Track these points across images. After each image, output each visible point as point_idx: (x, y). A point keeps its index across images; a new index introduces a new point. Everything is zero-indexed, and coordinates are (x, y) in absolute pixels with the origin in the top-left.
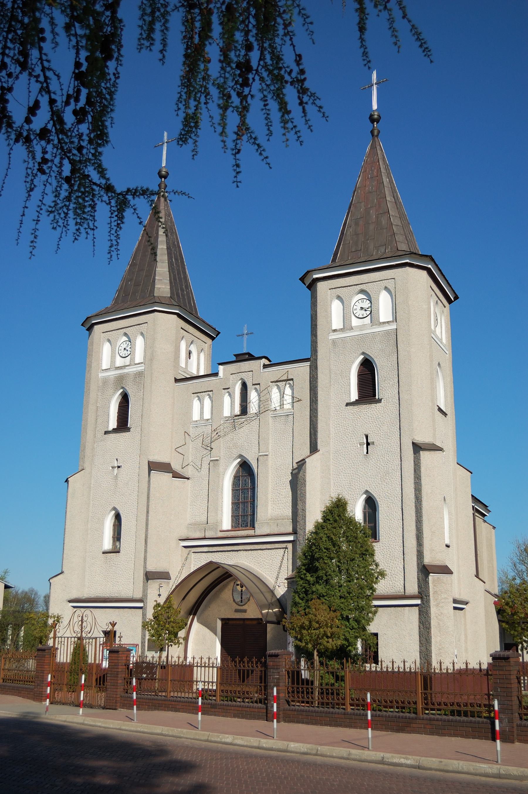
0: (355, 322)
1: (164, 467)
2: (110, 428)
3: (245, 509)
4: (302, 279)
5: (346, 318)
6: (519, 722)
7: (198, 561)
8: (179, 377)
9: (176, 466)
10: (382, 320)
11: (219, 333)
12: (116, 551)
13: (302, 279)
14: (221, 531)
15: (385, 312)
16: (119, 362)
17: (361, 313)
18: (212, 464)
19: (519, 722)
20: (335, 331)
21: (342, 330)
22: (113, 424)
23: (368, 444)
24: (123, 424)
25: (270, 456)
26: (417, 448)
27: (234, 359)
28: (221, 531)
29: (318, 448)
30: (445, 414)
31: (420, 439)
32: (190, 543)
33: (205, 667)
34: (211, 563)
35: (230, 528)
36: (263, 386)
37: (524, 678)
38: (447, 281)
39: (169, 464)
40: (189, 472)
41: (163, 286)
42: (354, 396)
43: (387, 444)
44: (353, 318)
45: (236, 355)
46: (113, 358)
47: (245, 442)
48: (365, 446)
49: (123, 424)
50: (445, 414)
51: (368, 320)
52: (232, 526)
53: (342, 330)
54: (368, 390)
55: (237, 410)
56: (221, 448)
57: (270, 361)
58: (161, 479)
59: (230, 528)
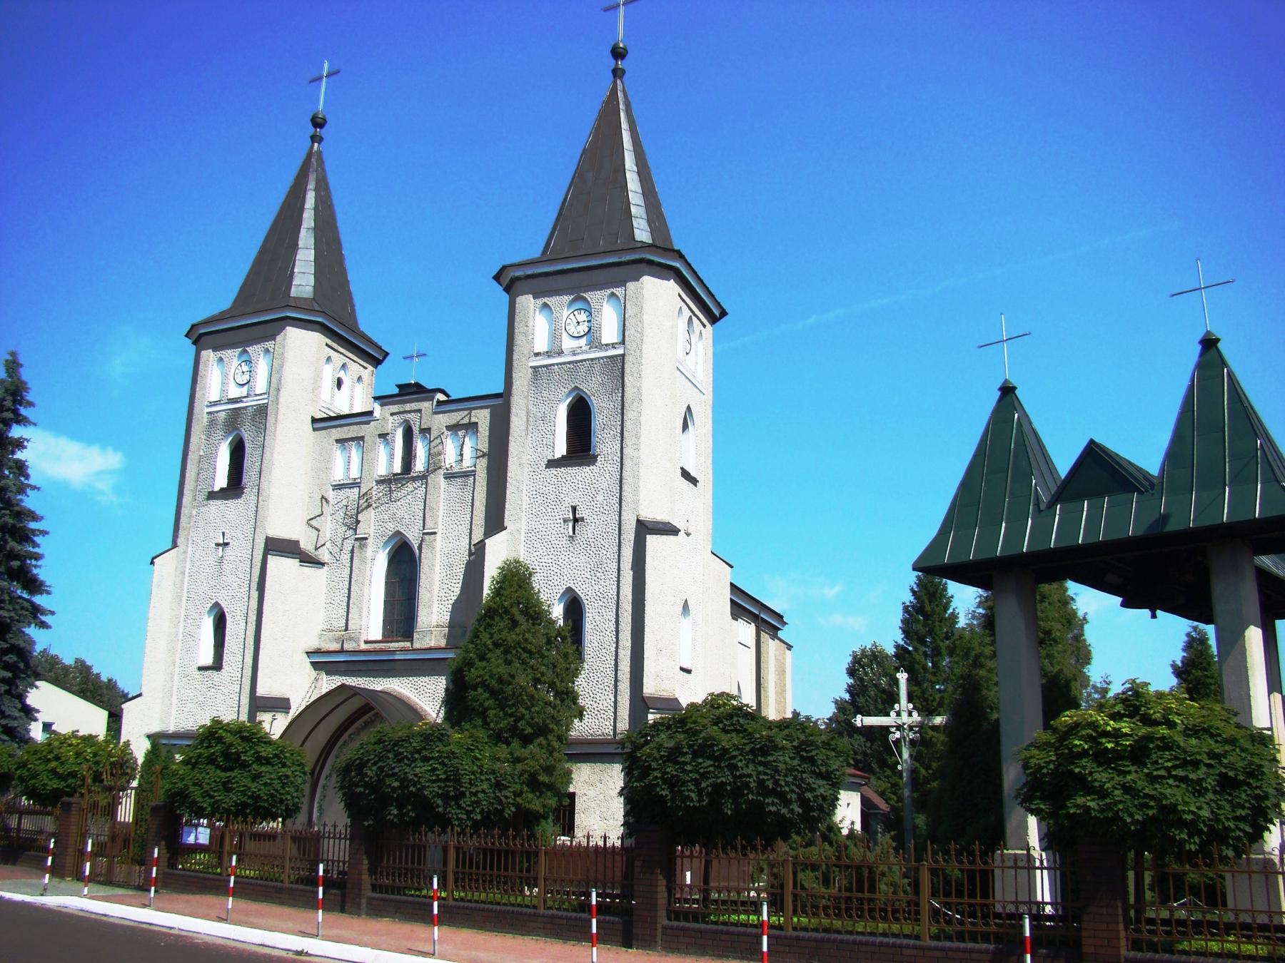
0: (568, 344)
1: (286, 548)
2: (217, 488)
3: (401, 612)
4: (497, 278)
5: (555, 335)
6: (666, 922)
7: (328, 683)
8: (319, 416)
9: (306, 545)
10: (604, 342)
11: (387, 354)
12: (217, 665)
13: (497, 278)
14: (366, 642)
15: (609, 333)
16: (234, 392)
17: (573, 330)
18: (357, 544)
19: (666, 922)
20: (537, 354)
21: (548, 354)
22: (221, 481)
23: (576, 520)
24: (235, 486)
25: (438, 537)
26: (645, 529)
27: (396, 391)
28: (366, 642)
29: (506, 524)
30: (694, 481)
31: (649, 514)
32: (322, 662)
33: (334, 837)
34: (343, 686)
35: (379, 637)
36: (434, 433)
37: (1139, 855)
38: (707, 288)
39: (297, 542)
40: (324, 555)
41: (303, 281)
42: (561, 449)
43: (598, 523)
44: (565, 335)
45: (399, 386)
46: (224, 384)
47: (403, 512)
48: (571, 525)
49: (235, 486)
50: (694, 481)
51: (583, 341)
52: (384, 635)
53: (548, 354)
54: (581, 446)
55: (397, 468)
56: (370, 523)
57: (447, 395)
58: (280, 566)
59: (379, 637)
